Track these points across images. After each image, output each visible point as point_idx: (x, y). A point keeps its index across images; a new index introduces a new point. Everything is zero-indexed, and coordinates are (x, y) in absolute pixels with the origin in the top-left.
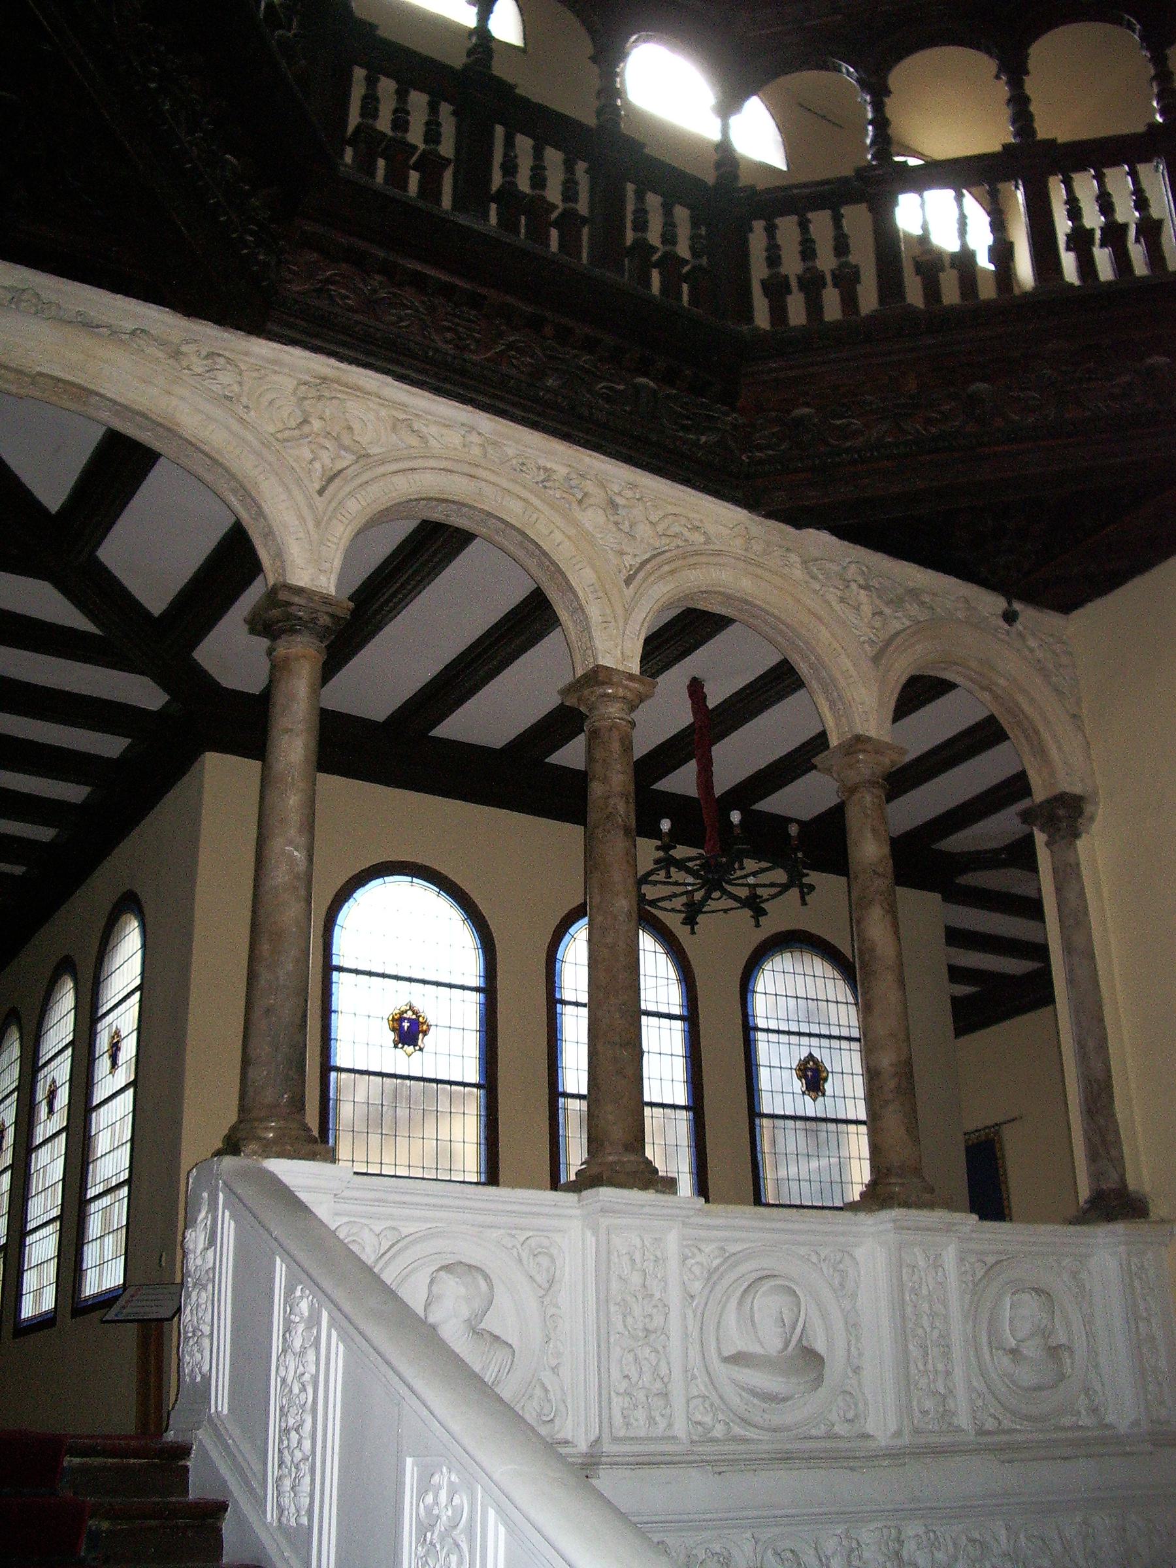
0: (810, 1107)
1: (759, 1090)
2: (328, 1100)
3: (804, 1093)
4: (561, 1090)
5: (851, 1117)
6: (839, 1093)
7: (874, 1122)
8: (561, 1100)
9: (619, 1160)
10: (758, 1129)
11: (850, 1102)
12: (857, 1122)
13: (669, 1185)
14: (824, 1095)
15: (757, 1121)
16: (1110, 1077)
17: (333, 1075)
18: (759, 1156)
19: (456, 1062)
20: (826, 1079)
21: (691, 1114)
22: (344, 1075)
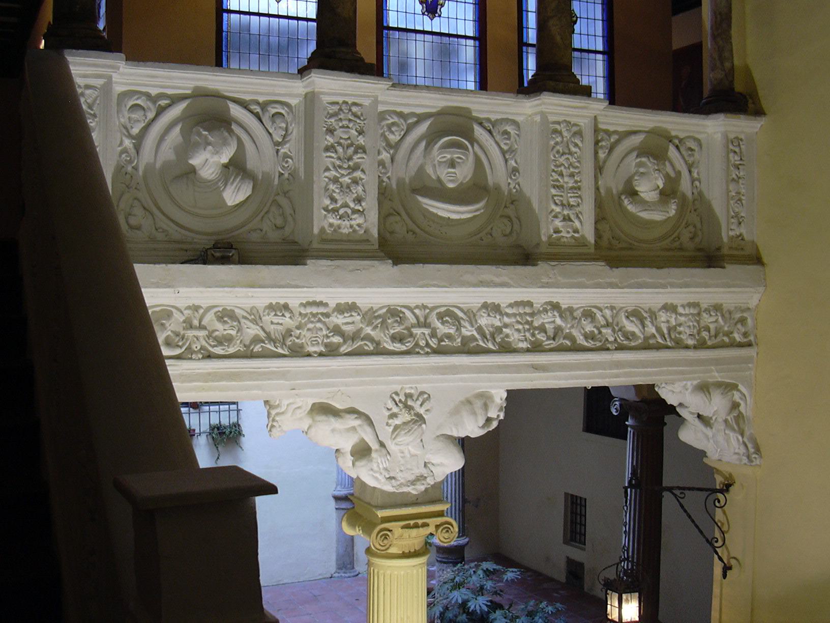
0: (427, 24)
1: (603, 37)
2: (222, 31)
3: (423, 14)
4: (385, 25)
5: (592, 48)
6: (584, 31)
7: (609, 52)
8: (385, 32)
9: (556, 76)
10: (524, 54)
11: (453, 22)
12: (599, 52)
13: (586, 92)
14: (440, 16)
15: (524, 49)
16: (731, 12)
17: (225, 15)
18: (525, 72)
19: (461, 23)
20: (575, 22)
21: (477, 43)
22: (233, 16)
